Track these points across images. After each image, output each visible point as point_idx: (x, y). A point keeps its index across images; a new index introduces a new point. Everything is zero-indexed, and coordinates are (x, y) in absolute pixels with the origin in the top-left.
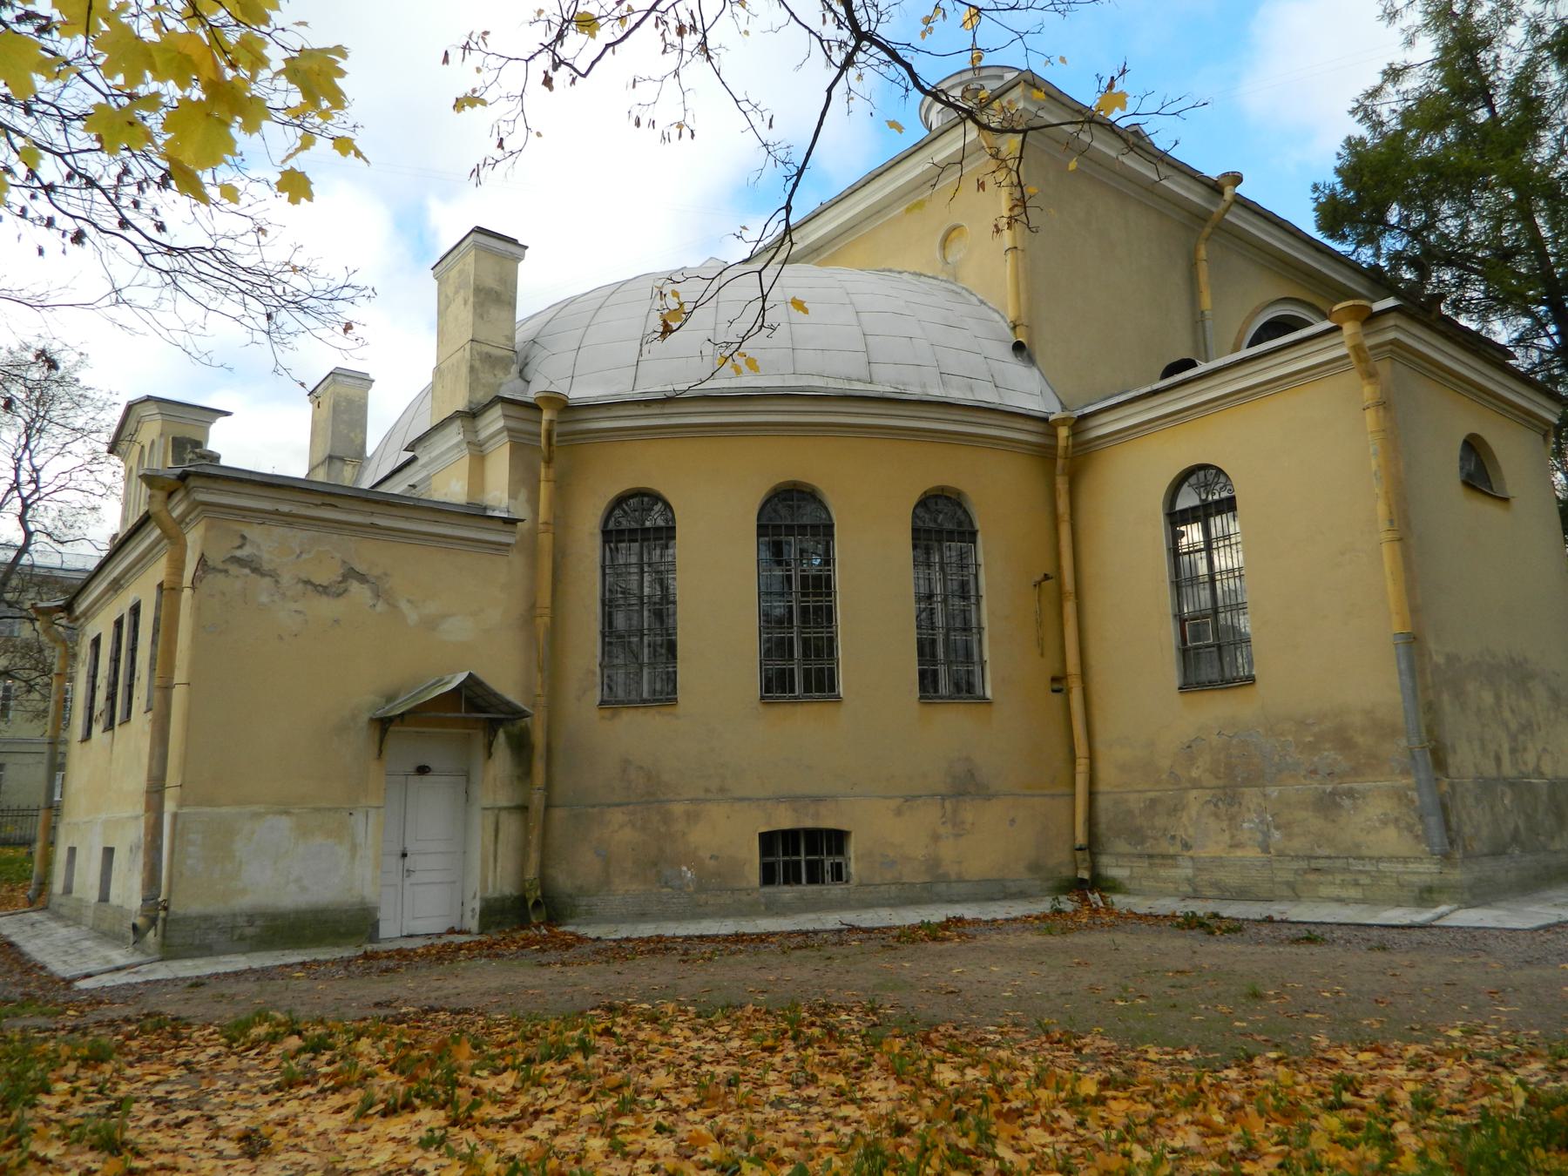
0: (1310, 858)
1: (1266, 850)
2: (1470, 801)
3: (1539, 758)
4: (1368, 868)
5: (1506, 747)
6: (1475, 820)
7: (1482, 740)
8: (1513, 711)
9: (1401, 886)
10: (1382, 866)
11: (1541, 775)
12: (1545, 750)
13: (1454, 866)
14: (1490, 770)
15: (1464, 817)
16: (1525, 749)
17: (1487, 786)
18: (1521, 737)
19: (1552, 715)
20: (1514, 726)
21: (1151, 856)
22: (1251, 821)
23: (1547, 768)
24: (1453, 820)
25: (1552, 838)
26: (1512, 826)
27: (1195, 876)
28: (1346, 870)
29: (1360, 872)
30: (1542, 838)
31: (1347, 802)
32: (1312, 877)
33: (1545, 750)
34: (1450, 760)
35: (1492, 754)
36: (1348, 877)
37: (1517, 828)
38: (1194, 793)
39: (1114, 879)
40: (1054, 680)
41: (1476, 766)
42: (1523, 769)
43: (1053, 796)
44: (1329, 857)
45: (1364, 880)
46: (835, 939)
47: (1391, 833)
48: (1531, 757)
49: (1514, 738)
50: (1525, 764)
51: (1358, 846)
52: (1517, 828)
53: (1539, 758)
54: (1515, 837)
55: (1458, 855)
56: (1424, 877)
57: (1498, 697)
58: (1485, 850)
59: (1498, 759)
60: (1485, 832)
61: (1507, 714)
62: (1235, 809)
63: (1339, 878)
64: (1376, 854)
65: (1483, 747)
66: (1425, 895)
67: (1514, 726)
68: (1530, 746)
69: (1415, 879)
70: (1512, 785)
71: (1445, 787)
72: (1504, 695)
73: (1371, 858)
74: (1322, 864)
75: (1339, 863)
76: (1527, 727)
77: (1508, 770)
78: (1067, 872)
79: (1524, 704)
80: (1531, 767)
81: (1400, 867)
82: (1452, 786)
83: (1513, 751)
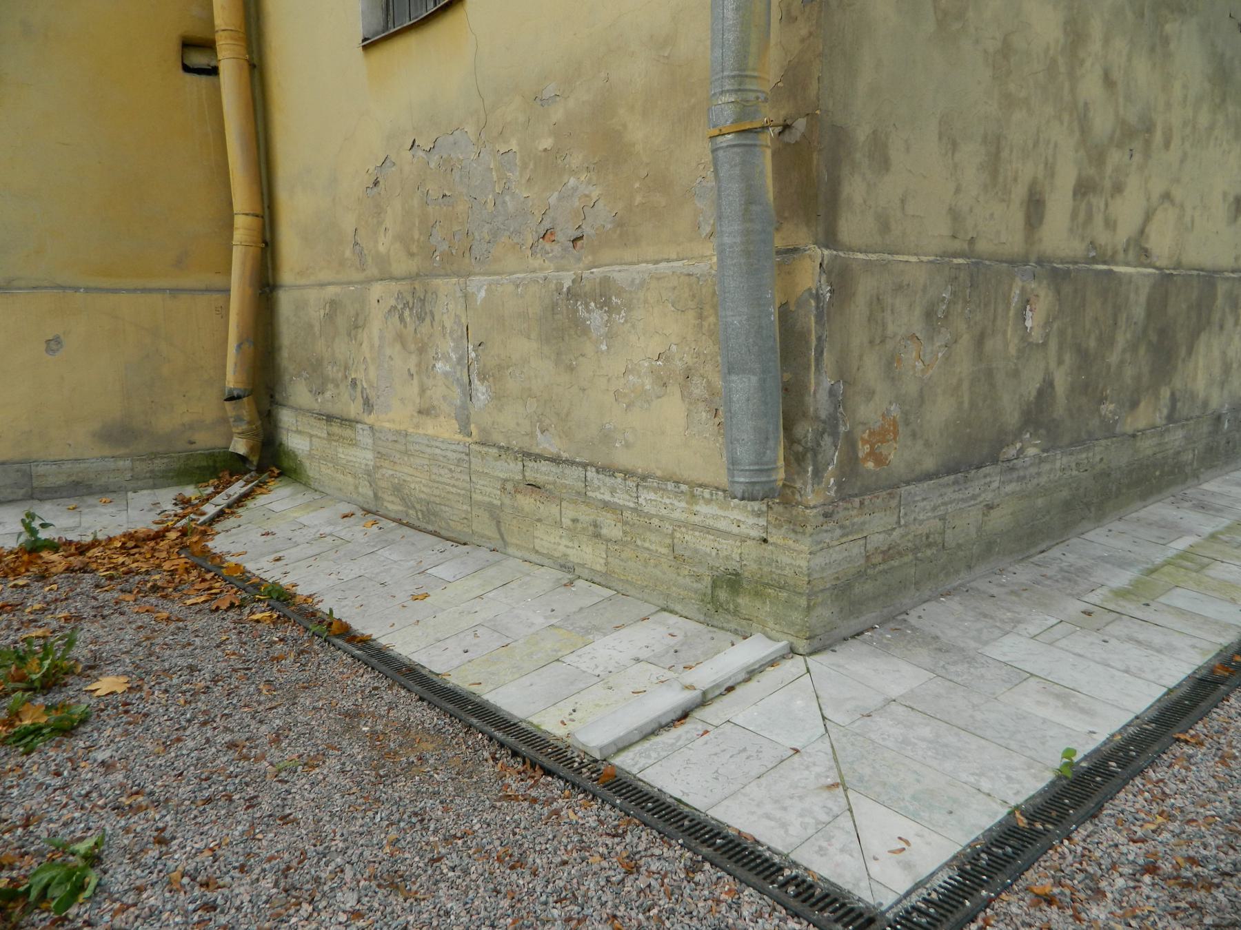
0: (527, 455)
1: (465, 429)
2: (905, 319)
3: (1148, 218)
4: (621, 499)
5: (1067, 177)
6: (907, 379)
7: (995, 148)
8: (1108, 81)
9: (678, 559)
10: (649, 499)
11: (1144, 255)
12: (1167, 196)
13: (797, 526)
14: (1000, 229)
15: (871, 370)
16: (1118, 189)
17: (974, 277)
18: (1115, 157)
19: (1204, 119)
20: (1102, 124)
21: (330, 418)
22: (447, 358)
23: (1162, 243)
24: (819, 389)
25: (1134, 405)
26: (1031, 386)
27: (377, 468)
28: (582, 497)
29: (606, 505)
30: (1108, 408)
31: (596, 318)
32: (527, 502)
33: (1167, 196)
34: (854, 188)
35: (1019, 192)
36: (586, 515)
37: (1048, 384)
38: (377, 290)
39: (292, 455)
40: (188, 45)
41: (955, 215)
42: (1103, 237)
43: (175, 291)
44: (556, 460)
45: (611, 529)
46: (391, 438)
47: (672, 408)
48: (1128, 211)
49: (1098, 157)
50: (1110, 224)
51: (606, 437)
52: (1046, 390)
53: (1148, 218)
54: (1037, 416)
55: (812, 496)
56: (726, 546)
57: (1075, 35)
58: (929, 464)
59: (1035, 206)
60: (940, 412)
61: (1091, 87)
62: (425, 328)
63: (569, 512)
64: (640, 466)
65: (993, 164)
66: (723, 595)
67: (1102, 124)
68: (1133, 183)
69: (705, 544)
70: (1058, 275)
71: (808, 276)
72: (1096, 28)
73: (628, 474)
74: (542, 472)
75: (573, 476)
76: (1138, 133)
77: (1058, 236)
78: (206, 440)
79: (1142, 68)
80: (1124, 233)
81: (679, 509)
82: (841, 279)
83: (1083, 188)
